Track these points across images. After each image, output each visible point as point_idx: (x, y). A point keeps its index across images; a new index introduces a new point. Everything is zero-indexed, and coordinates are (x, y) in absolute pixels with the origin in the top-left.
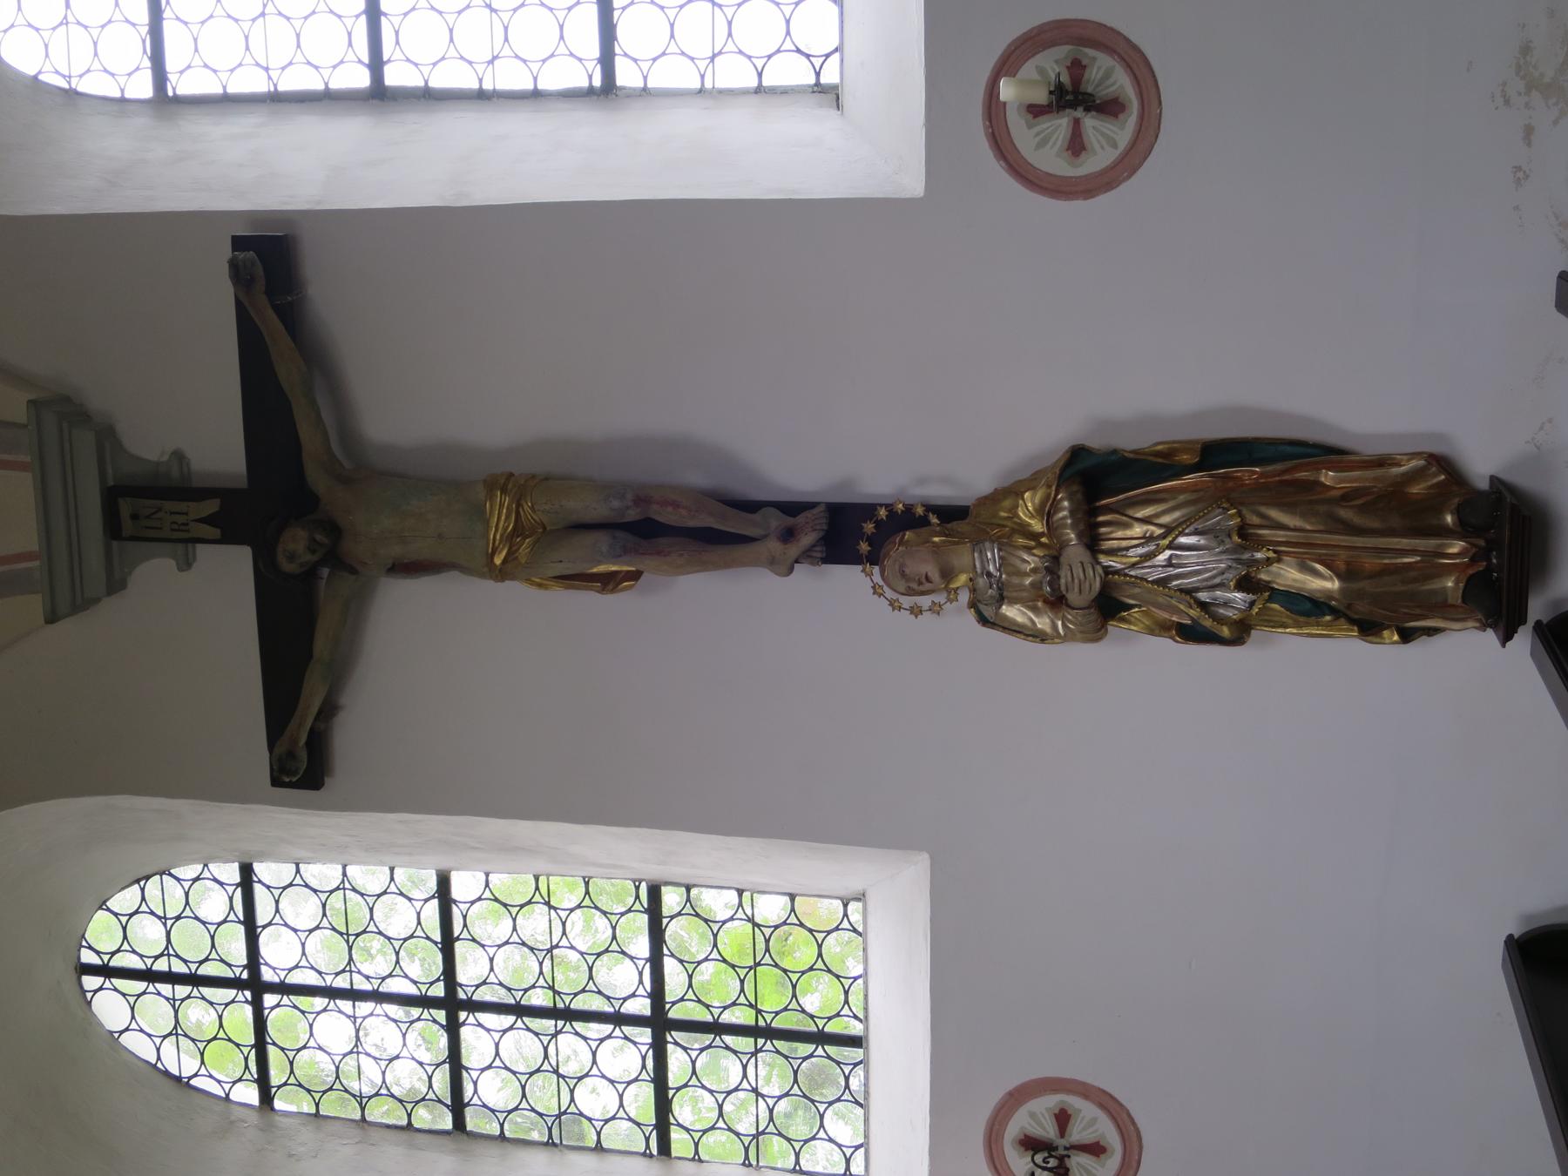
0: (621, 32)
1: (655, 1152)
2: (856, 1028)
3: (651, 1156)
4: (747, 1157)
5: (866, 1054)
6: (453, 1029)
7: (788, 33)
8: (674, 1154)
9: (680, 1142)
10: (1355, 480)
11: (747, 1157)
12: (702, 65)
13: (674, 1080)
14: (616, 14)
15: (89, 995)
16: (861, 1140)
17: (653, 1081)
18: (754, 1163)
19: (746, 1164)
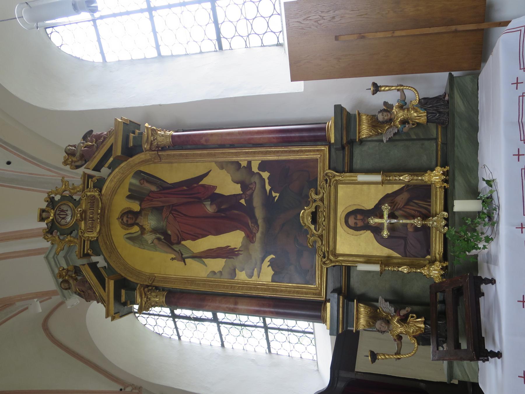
0: (222, 31)
1: (218, 49)
2: (312, 331)
3: (217, 51)
4: (246, 45)
5: (315, 336)
6: (151, 18)
7: (268, 23)
8: (224, 49)
9: (225, 45)
10: (435, 248)
11: (246, 45)
12: (245, 38)
13: (270, 339)
14: (220, 25)
15: (49, 35)
16: (281, 30)
17: (214, 22)
18: (248, 46)
19: (246, 47)
